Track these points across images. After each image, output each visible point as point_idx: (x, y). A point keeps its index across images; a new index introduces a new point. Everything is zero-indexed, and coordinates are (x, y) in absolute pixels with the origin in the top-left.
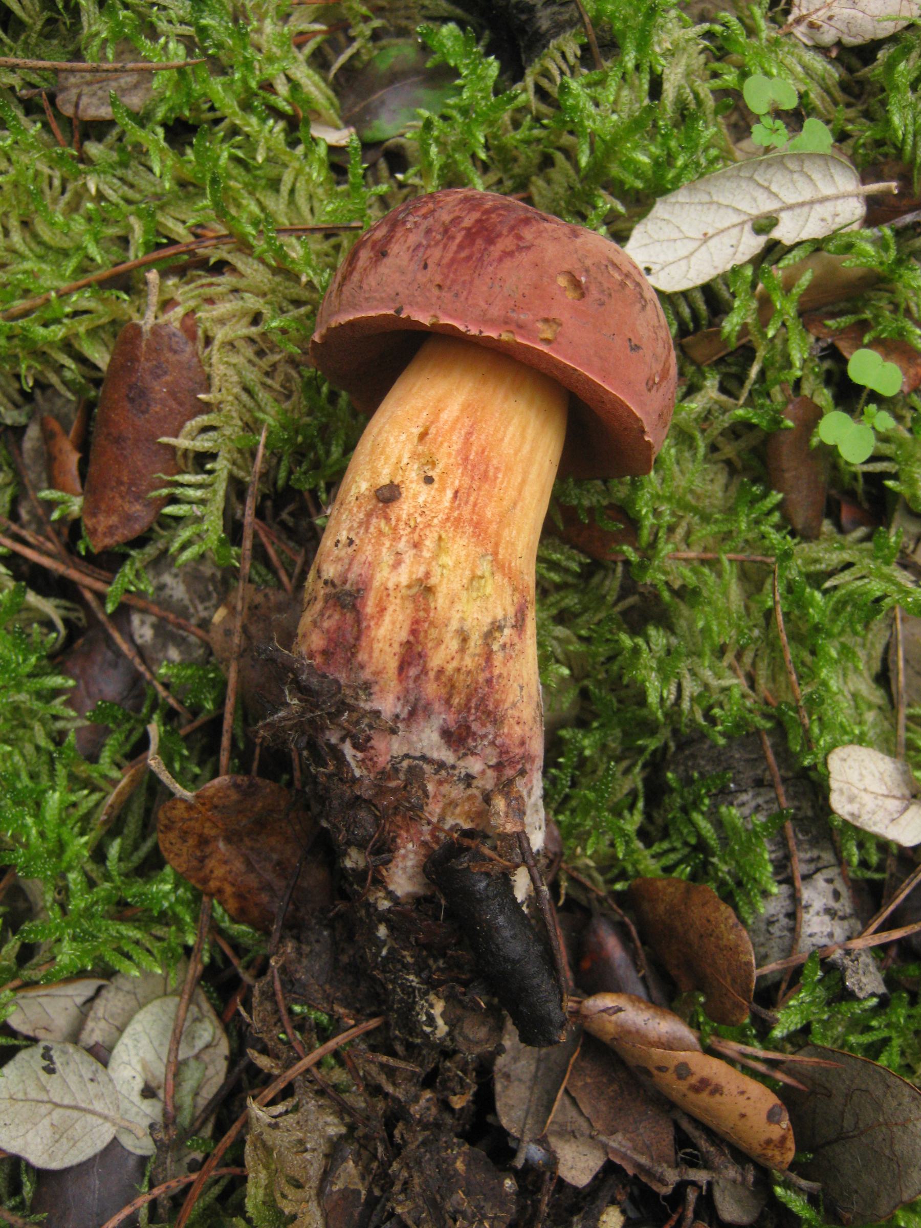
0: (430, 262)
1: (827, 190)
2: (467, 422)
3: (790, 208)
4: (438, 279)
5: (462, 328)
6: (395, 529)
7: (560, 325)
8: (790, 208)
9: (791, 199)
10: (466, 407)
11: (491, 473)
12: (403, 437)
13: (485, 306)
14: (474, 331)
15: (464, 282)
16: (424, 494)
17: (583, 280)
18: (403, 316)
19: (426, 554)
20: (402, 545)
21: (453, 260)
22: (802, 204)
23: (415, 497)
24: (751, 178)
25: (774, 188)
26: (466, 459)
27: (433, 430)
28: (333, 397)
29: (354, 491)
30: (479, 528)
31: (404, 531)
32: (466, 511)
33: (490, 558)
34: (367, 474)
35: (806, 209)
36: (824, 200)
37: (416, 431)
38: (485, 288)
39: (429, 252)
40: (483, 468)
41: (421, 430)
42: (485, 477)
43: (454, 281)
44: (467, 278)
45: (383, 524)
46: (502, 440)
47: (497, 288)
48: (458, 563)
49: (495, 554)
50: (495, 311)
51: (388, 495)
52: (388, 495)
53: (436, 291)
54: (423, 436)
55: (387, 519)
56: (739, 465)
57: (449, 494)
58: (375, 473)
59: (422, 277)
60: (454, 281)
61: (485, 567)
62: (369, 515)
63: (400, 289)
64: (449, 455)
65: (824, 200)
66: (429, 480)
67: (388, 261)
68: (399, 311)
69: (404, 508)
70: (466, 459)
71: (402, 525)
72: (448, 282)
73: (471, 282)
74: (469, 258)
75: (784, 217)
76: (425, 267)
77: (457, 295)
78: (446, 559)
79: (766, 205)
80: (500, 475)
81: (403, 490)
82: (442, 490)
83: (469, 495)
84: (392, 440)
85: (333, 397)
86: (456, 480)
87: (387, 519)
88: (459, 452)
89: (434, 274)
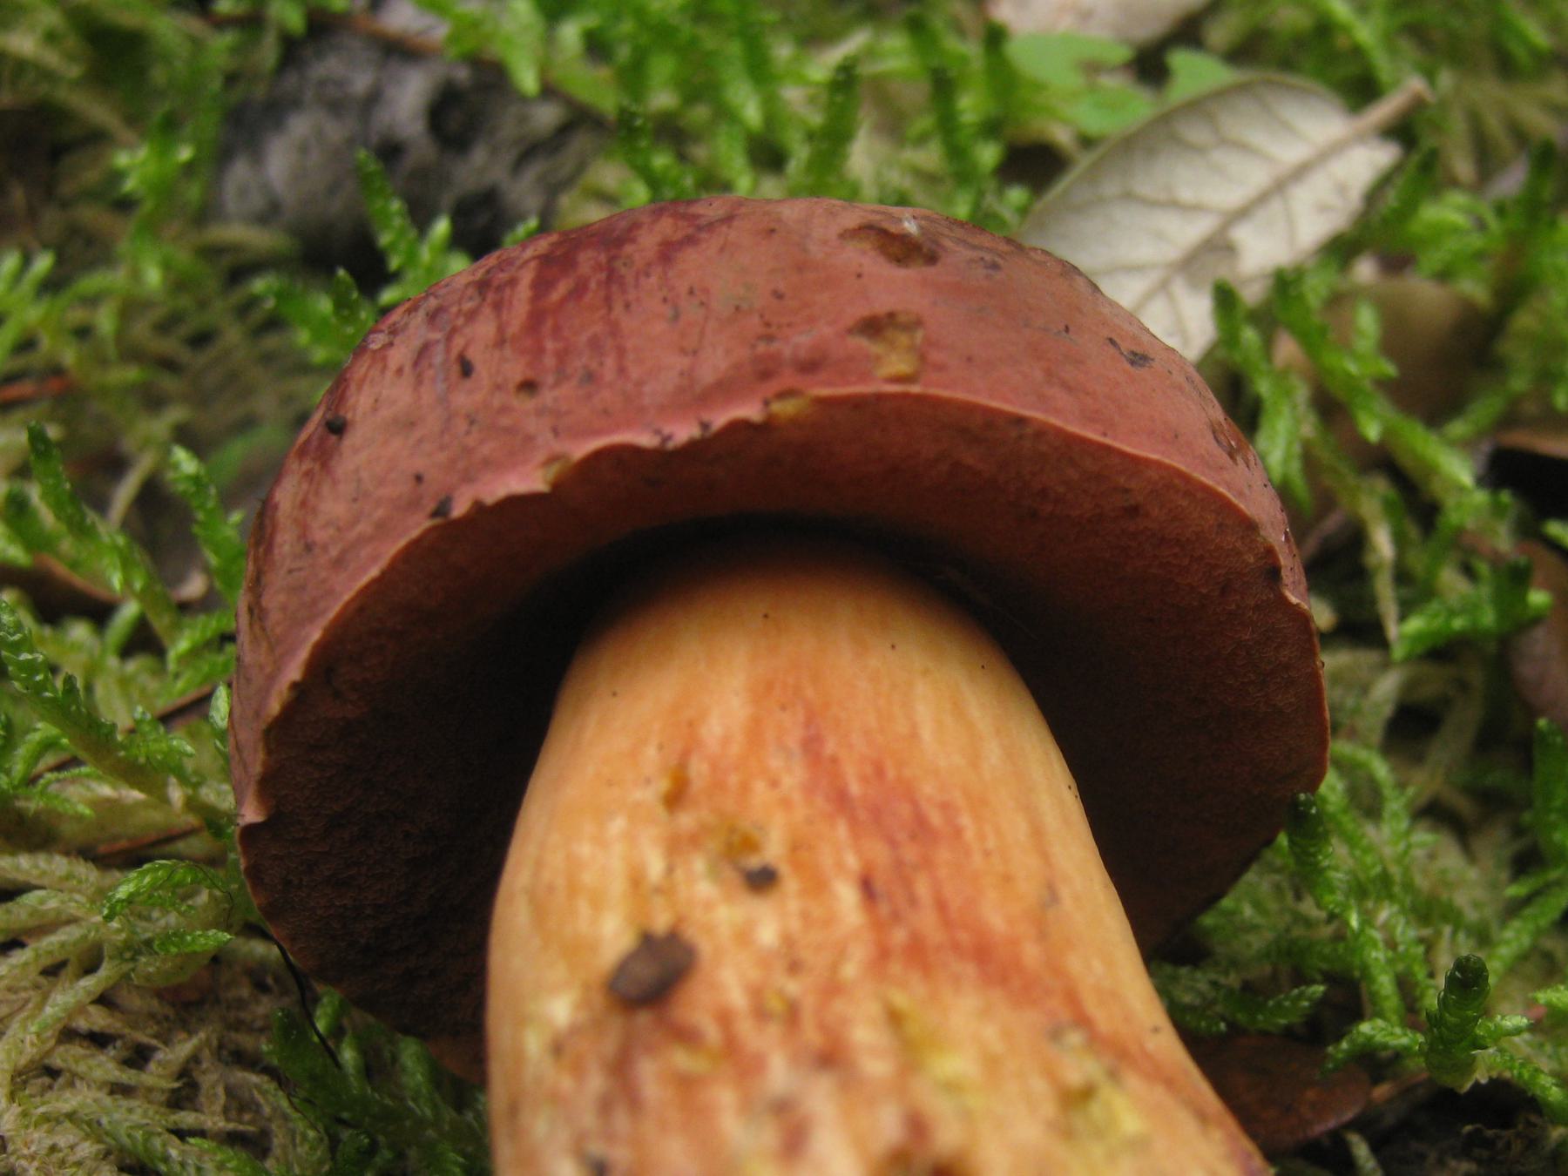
0: (475, 355)
1: (1290, 153)
2: (792, 726)
3: (1242, 213)
4: (516, 370)
5: (646, 440)
6: (731, 1048)
7: (918, 323)
8: (1242, 213)
9: (1230, 196)
10: (761, 692)
11: (935, 818)
12: (618, 825)
13: (683, 362)
14: (683, 432)
15: (595, 344)
16: (768, 923)
17: (911, 227)
18: (459, 509)
19: (876, 1066)
20: (779, 1074)
21: (536, 319)
22: (1262, 199)
23: (744, 936)
24: (1128, 197)
25: (1186, 194)
26: (841, 800)
27: (698, 770)
28: (376, 1067)
29: (534, 1044)
30: (992, 963)
31: (767, 1042)
32: (927, 921)
33: (1075, 1038)
34: (559, 972)
35: (1275, 206)
36: (1301, 172)
37: (649, 795)
38: (659, 327)
39: (459, 342)
40: (905, 810)
41: (663, 785)
42: (921, 829)
43: (562, 356)
44: (598, 328)
45: (682, 1059)
46: (914, 735)
47: (692, 311)
48: (992, 1064)
49: (1082, 1021)
50: (715, 363)
51: (653, 982)
52: (653, 982)
53: (526, 404)
54: (676, 798)
55: (687, 1037)
56: (1464, 806)
57: (847, 896)
58: (576, 950)
59: (465, 398)
60: (562, 356)
61: (1079, 1068)
62: (621, 1068)
63: (419, 464)
64: (786, 803)
65: (1301, 172)
66: (762, 881)
67: (352, 439)
68: (441, 510)
69: (726, 982)
70: (841, 800)
71: (746, 1028)
72: (549, 361)
73: (614, 330)
74: (579, 290)
75: (1243, 234)
76: (466, 369)
77: (591, 377)
78: (955, 1064)
79: (1188, 232)
80: (965, 820)
81: (691, 933)
82: (817, 886)
83: (908, 884)
84: (585, 850)
85: (376, 1067)
86: (842, 855)
87: (687, 1037)
88: (809, 790)
89: (498, 367)
